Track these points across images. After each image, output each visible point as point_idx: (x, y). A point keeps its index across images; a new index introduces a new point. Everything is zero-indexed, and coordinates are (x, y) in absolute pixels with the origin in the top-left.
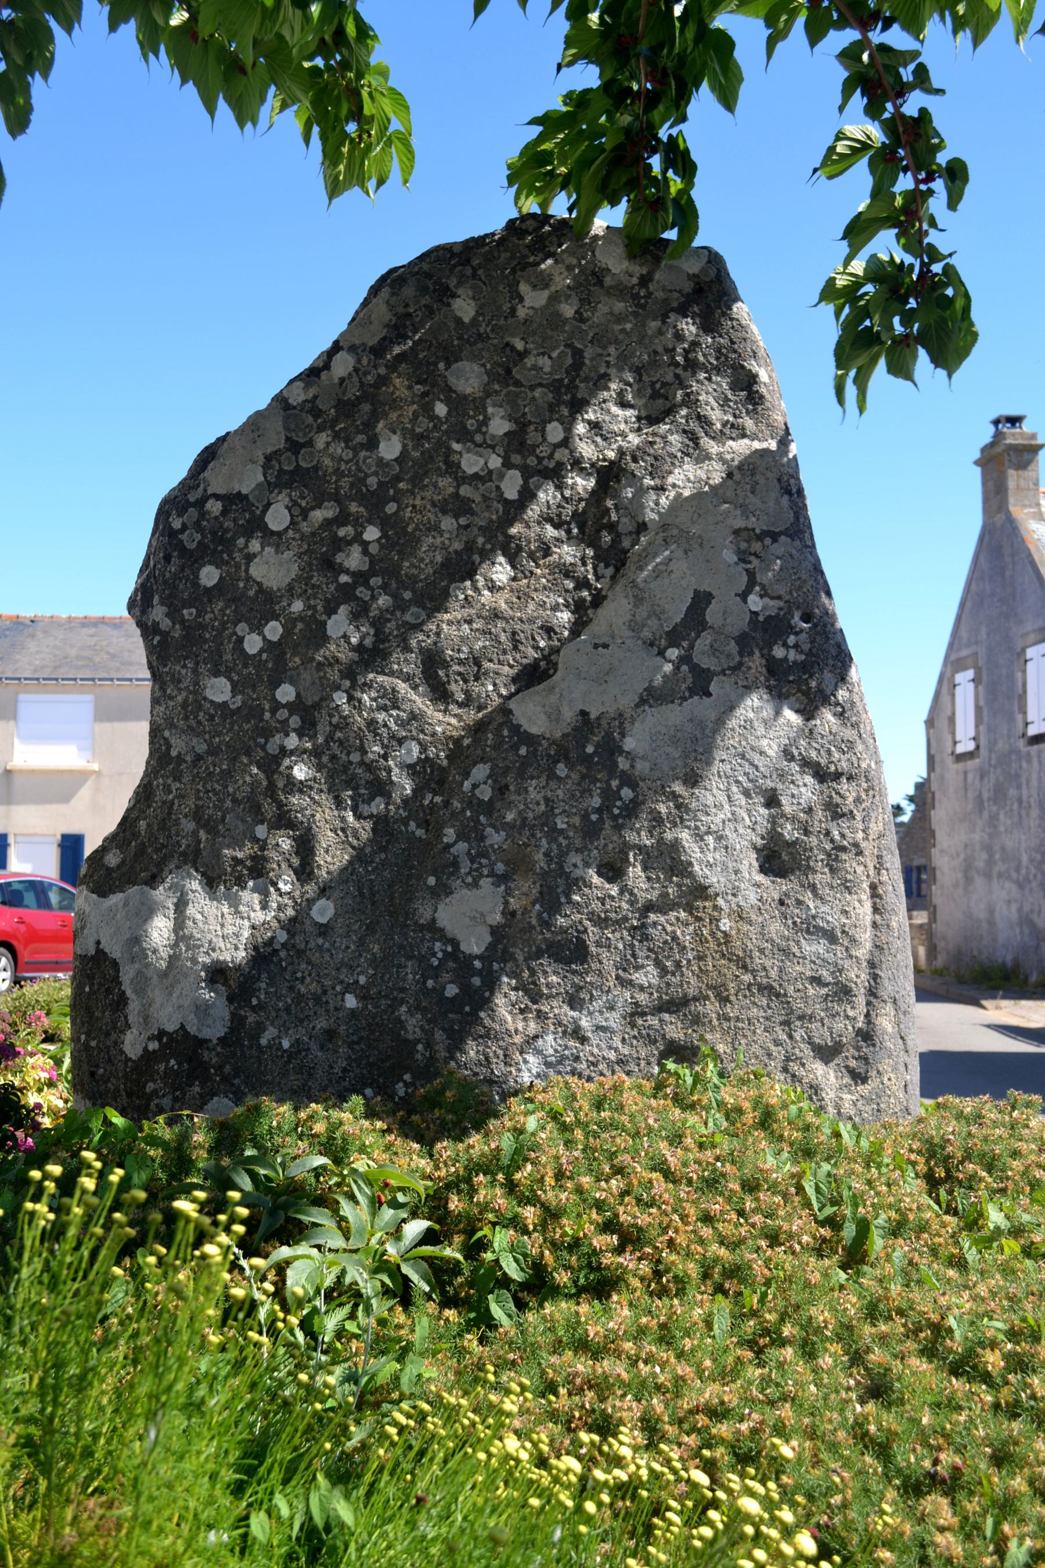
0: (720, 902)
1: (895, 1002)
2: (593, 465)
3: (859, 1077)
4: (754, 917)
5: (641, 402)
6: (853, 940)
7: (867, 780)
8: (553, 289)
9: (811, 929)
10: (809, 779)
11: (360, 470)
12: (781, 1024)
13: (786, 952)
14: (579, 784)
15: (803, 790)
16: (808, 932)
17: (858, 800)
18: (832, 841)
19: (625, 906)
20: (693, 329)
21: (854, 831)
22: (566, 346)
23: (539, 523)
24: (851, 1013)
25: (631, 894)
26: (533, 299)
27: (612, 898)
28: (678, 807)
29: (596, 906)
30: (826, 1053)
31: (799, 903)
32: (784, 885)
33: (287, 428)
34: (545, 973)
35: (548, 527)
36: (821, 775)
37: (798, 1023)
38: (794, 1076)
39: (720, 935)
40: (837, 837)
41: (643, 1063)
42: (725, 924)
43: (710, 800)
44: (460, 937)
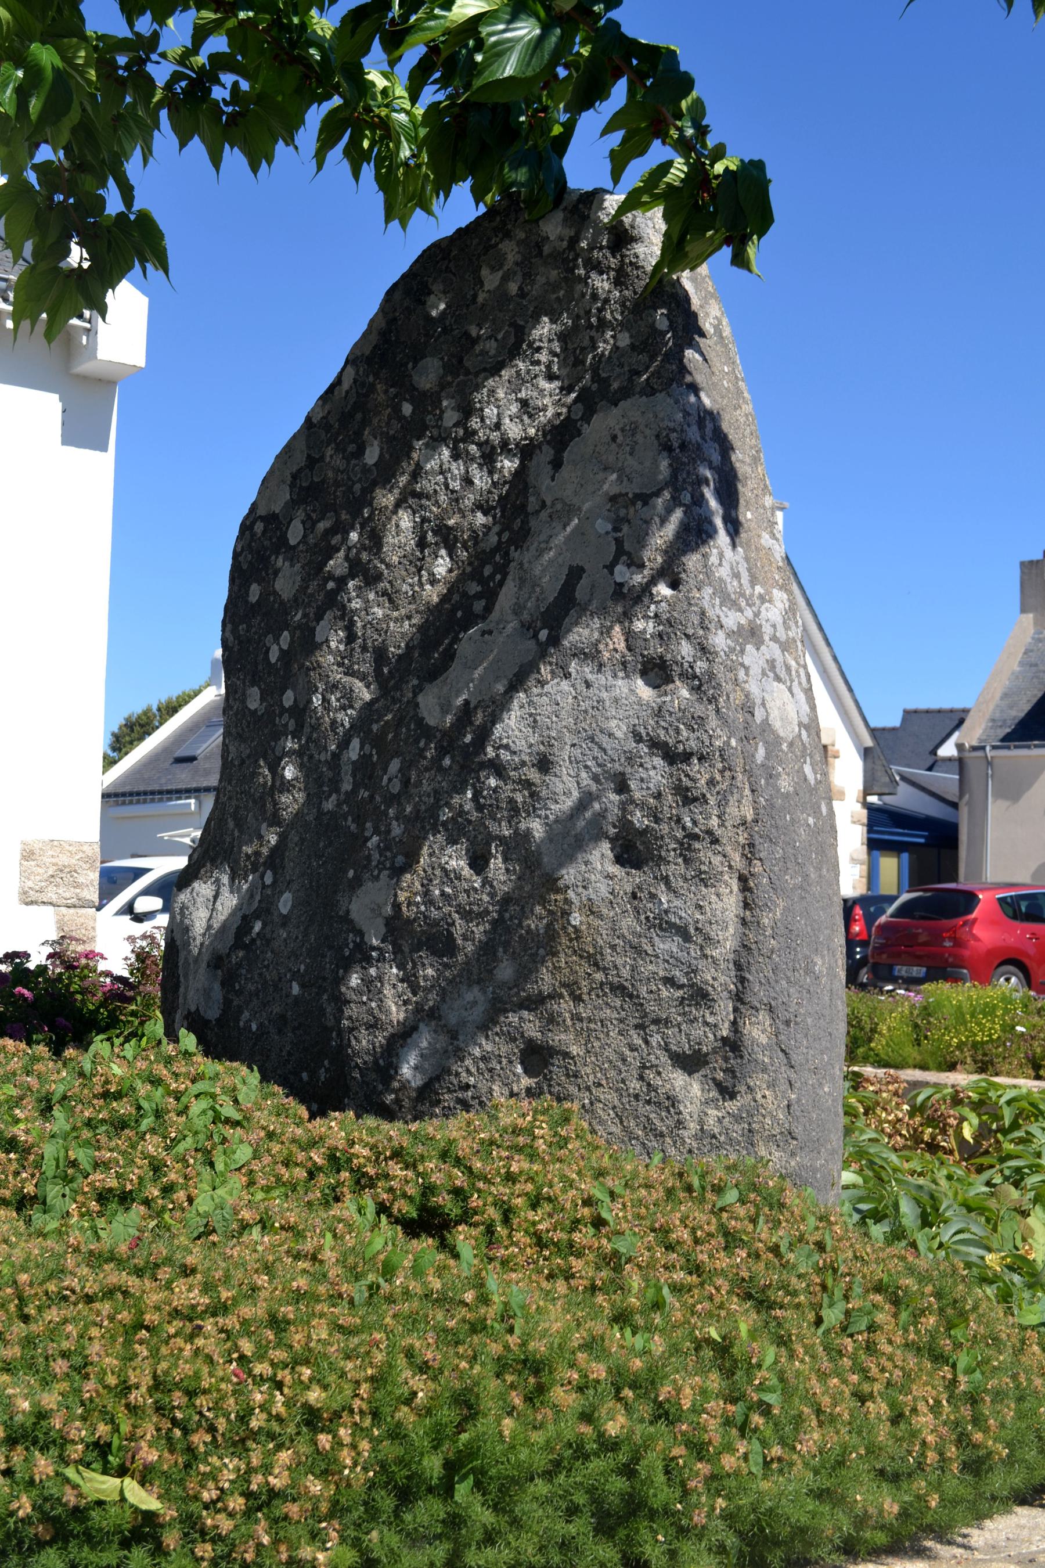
0: (571, 894)
1: (771, 1010)
2: (517, 445)
3: (727, 1092)
4: (605, 911)
5: (564, 372)
6: (708, 938)
7: (723, 760)
8: (506, 268)
9: (664, 925)
10: (658, 761)
11: (349, 479)
12: (637, 1027)
13: (638, 950)
14: (459, 775)
15: (652, 773)
16: (661, 929)
17: (711, 782)
18: (684, 828)
19: (486, 898)
20: (606, 286)
21: (708, 818)
22: (510, 325)
23: (473, 511)
24: (710, 1019)
25: (492, 886)
26: (491, 280)
27: (475, 890)
28: (532, 795)
29: (463, 898)
30: (690, 1062)
31: (653, 896)
32: (638, 877)
33: (309, 447)
34: (424, 965)
35: (479, 514)
36: (674, 757)
37: (652, 1027)
38: (649, 1085)
39: (571, 929)
40: (689, 824)
41: (504, 1061)
42: (576, 919)
43: (559, 788)
44: (364, 929)
